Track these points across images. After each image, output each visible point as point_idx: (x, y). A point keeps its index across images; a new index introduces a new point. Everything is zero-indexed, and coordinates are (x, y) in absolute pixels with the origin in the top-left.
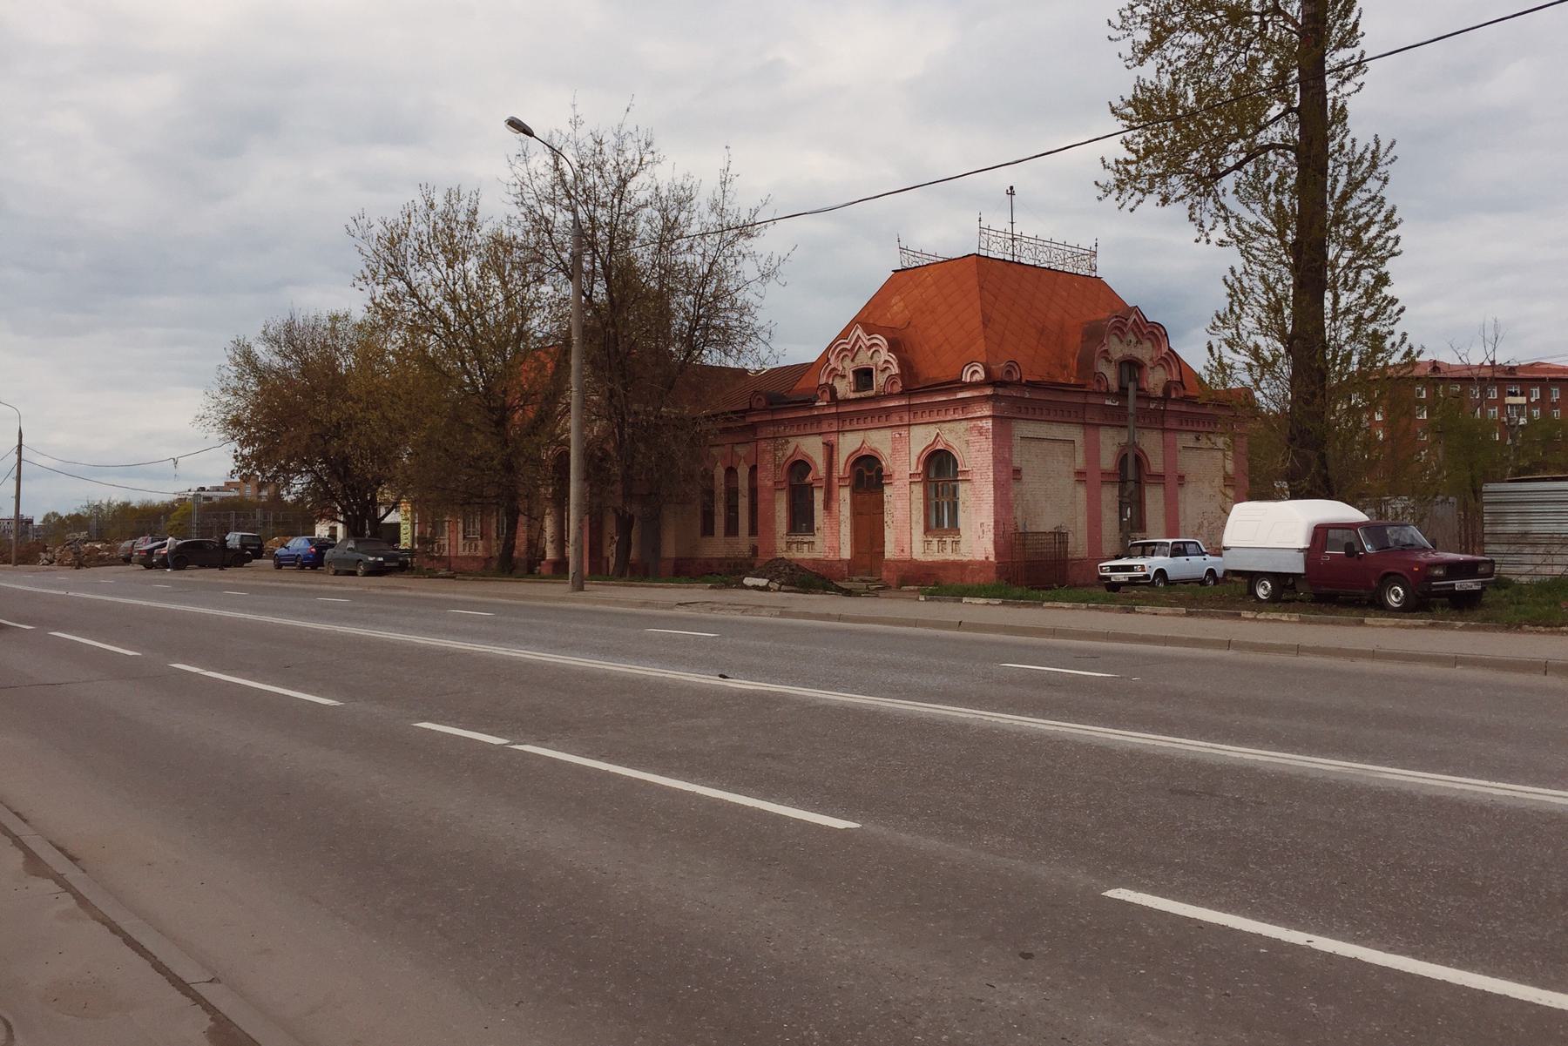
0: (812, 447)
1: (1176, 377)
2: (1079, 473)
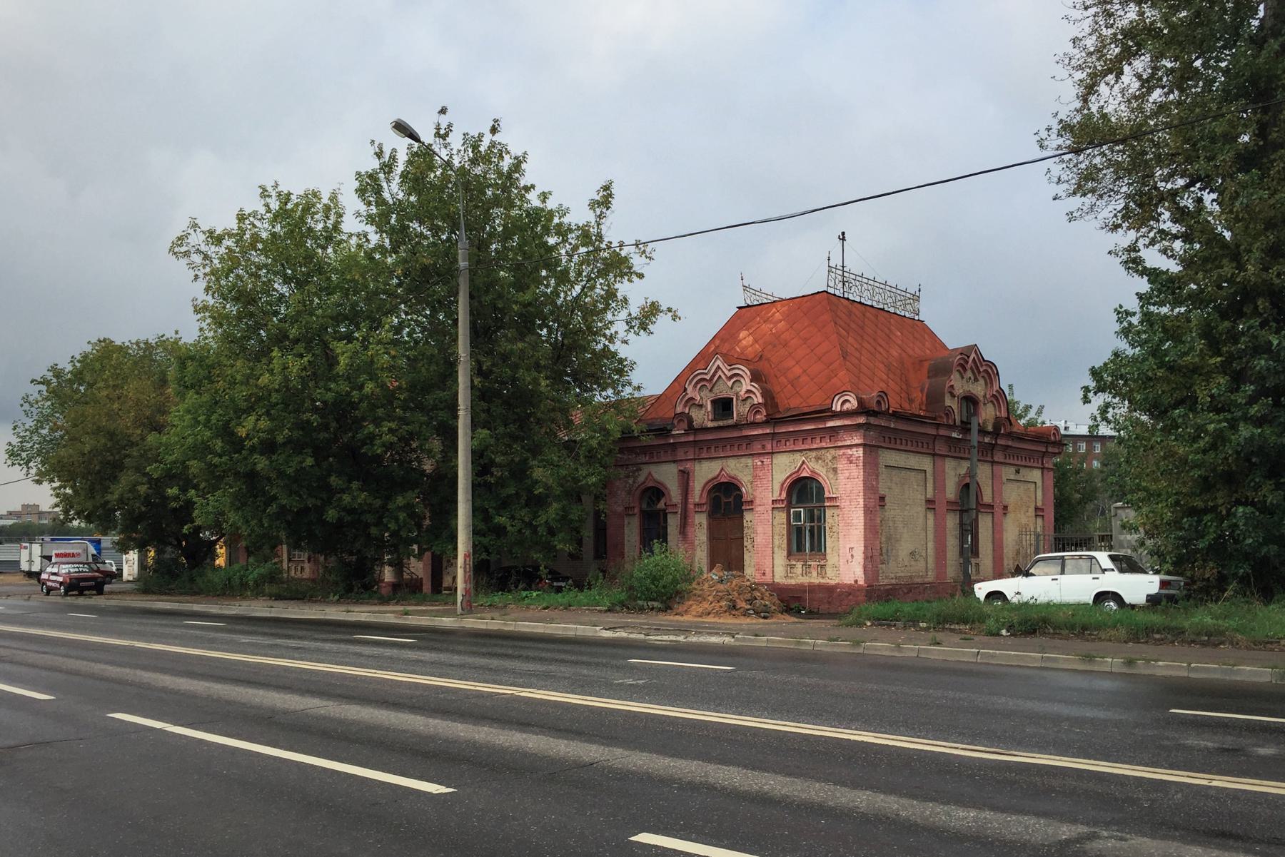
0: (667, 475)
1: (1004, 414)
2: (929, 502)
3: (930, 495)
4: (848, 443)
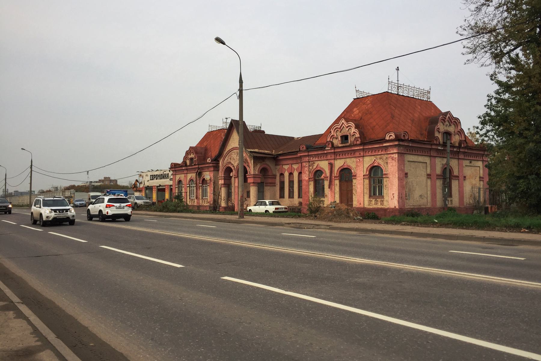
0: (324, 165)
3: (429, 172)
4: (392, 152)
